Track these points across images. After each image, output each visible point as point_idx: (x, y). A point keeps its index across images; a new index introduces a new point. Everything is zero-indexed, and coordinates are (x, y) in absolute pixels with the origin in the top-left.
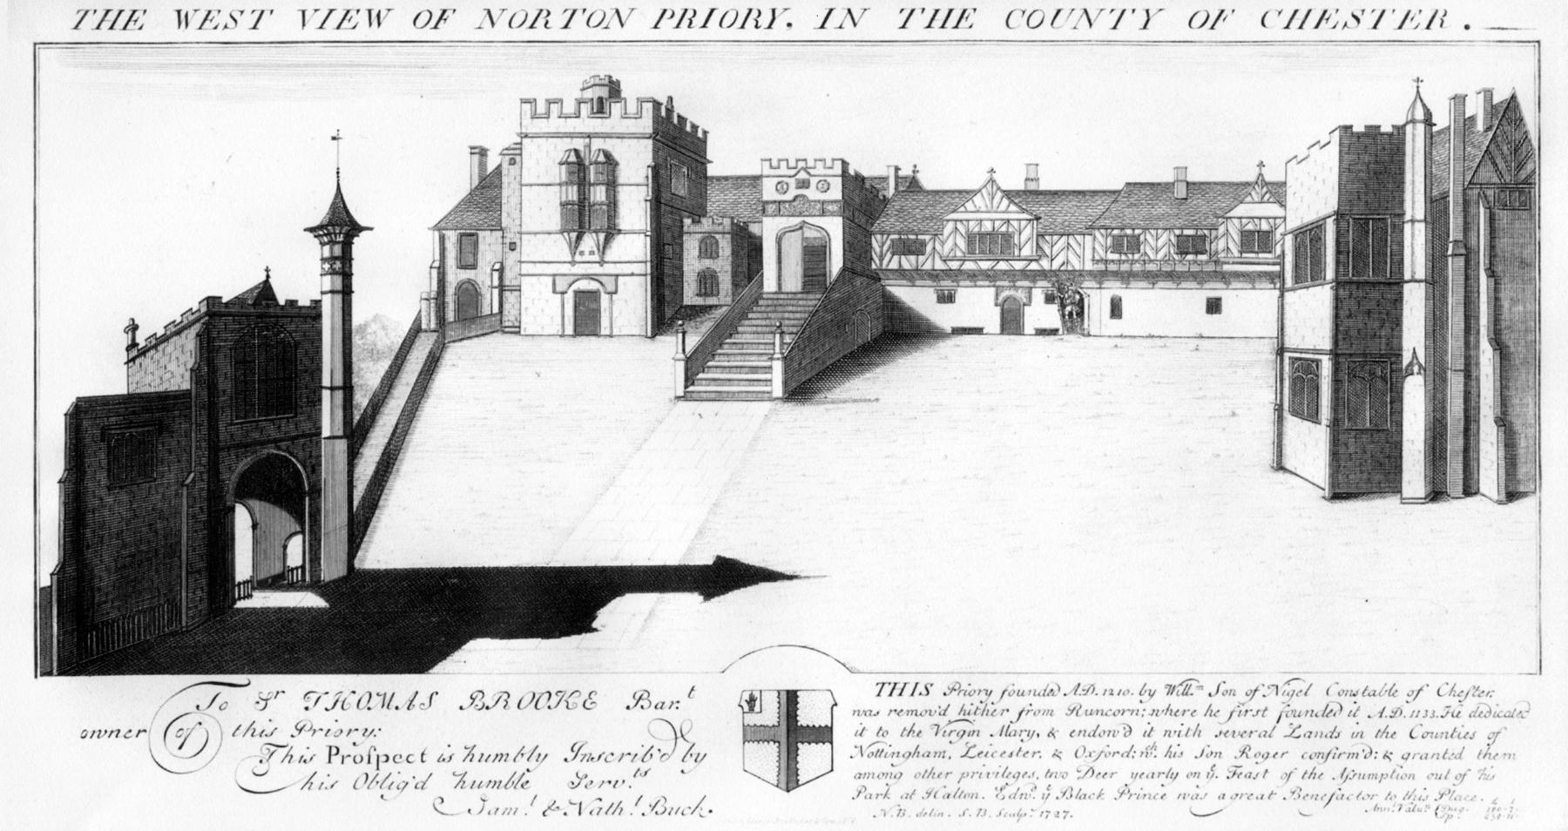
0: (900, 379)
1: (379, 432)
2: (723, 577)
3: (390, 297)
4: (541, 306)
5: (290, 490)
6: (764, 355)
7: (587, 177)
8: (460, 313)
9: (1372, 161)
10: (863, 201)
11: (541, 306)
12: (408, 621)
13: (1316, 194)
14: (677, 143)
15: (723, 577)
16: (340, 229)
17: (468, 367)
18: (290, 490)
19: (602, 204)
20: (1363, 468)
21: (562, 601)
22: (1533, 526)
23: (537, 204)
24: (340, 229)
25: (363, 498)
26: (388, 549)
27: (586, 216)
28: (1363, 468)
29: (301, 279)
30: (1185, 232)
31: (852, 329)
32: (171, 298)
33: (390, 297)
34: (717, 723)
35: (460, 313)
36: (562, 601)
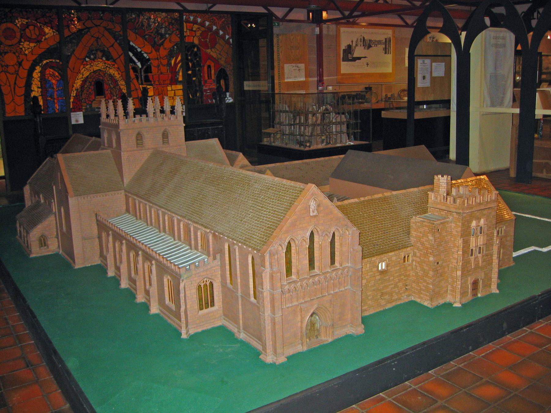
0: (371, 49)
1: (354, 50)
2: (365, 57)
3: (354, 45)
4: (359, 45)
5: (350, 53)
6: (367, 47)
7: (361, 39)
8: (357, 45)
9: (386, 39)
10: (370, 41)
11: (359, 45)
12: (355, 59)
13: (384, 41)
14: (364, 38)
15: (365, 57)
16: (352, 41)
17: (357, 47)
18: (350, 53)
19: (394, 32)
20: (386, 53)
21: (359, 58)
22: (429, 54)
23: (359, 41)
24: (352, 41)
25: (532, 40)
26: (354, 56)
27: (361, 41)
28: (386, 53)
29: (351, 44)
30: (379, 42)
31: (369, 47)
32: (346, 45)
33: (354, 45)
34: (365, 64)
35: (357, 45)
36: (359, 58)
